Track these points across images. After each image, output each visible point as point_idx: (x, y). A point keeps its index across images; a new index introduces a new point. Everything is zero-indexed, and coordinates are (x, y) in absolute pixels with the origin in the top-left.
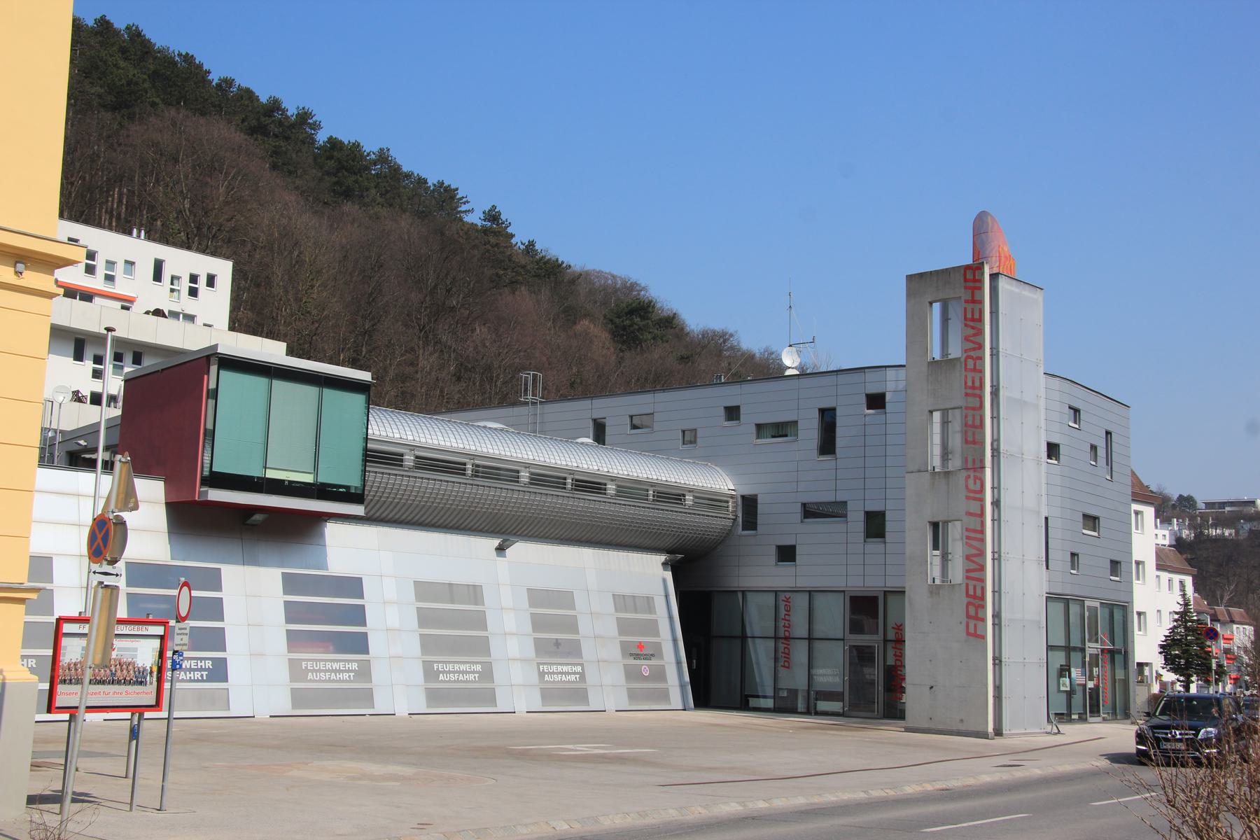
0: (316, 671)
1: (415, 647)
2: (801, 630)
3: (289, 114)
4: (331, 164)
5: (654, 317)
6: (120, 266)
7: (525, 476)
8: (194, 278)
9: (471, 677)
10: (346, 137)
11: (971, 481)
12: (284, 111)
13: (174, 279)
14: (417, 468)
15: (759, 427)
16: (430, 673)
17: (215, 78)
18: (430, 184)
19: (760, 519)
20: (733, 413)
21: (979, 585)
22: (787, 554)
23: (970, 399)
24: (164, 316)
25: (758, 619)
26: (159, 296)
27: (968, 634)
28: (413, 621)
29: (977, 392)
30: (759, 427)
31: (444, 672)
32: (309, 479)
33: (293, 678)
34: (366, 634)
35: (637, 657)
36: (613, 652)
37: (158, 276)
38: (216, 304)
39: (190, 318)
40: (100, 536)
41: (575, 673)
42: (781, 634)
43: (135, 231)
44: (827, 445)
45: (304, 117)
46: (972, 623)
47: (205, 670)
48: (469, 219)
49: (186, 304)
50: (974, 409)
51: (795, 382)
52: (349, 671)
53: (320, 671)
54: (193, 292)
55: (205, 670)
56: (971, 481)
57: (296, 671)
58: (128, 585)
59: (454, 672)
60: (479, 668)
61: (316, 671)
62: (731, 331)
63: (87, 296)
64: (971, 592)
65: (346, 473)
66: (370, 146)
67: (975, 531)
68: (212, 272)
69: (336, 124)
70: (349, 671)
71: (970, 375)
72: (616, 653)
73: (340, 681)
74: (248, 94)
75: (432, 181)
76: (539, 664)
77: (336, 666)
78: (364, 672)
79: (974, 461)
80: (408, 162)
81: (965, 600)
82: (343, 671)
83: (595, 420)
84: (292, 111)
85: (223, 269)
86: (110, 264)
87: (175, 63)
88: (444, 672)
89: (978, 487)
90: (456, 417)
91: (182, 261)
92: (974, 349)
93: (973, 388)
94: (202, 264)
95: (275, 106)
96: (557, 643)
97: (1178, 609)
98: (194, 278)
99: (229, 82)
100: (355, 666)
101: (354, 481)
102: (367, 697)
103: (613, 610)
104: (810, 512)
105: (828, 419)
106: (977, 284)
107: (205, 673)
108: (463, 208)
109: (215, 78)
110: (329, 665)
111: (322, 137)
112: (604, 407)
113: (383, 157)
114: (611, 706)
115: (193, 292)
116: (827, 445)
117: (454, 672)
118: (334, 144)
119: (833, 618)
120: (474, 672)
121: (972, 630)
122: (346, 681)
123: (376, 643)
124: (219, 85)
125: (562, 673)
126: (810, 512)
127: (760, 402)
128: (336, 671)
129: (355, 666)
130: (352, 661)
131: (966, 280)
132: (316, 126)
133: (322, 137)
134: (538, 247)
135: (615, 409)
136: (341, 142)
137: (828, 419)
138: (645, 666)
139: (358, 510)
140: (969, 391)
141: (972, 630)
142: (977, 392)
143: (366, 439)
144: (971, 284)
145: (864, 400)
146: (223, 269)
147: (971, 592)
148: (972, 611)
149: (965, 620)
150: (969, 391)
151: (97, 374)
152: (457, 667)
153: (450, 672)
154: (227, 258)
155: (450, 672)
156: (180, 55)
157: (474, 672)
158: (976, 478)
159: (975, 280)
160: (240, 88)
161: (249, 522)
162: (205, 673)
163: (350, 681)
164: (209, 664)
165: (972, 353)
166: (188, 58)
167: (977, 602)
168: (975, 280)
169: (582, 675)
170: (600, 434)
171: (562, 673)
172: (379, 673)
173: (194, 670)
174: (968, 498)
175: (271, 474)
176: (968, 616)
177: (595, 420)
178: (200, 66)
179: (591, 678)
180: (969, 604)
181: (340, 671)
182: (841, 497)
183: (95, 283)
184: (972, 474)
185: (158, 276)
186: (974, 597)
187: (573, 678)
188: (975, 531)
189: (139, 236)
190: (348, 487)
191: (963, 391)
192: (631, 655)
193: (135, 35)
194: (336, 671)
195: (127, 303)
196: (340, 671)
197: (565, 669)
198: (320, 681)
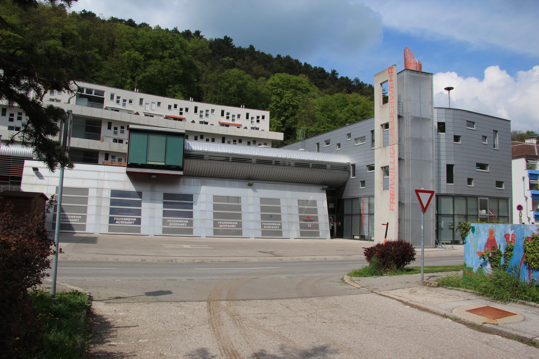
1: (259, 218)
6: (261, 118)
7: (254, 161)
8: (258, 117)
9: (233, 226)
13: (252, 118)
16: (216, 224)
19: (455, 179)
20: (349, 135)
26: (247, 123)
28: (259, 210)
32: (163, 164)
33: (214, 226)
36: (296, 219)
37: (247, 118)
38: (265, 124)
46: (391, 204)
49: (256, 125)
54: (258, 121)
57: (165, 222)
60: (236, 223)
63: (227, 125)
68: (187, 107)
71: (391, 109)
72: (297, 219)
76: (262, 223)
78: (191, 223)
81: (390, 196)
85: (267, 114)
86: (233, 116)
90: (286, 147)
91: (254, 113)
94: (260, 113)
96: (271, 216)
98: (258, 117)
110: (177, 221)
111: (339, 77)
113: (357, 80)
114: (203, 235)
115: (258, 121)
128: (180, 223)
130: (186, 220)
139: (181, 173)
143: (184, 151)
146: (267, 114)
149: (389, 204)
176: (391, 203)
179: (284, 227)
180: (391, 198)
181: (181, 223)
183: (229, 121)
185: (247, 118)
193: (288, 58)
194: (180, 223)
195: (239, 126)
196: (181, 223)
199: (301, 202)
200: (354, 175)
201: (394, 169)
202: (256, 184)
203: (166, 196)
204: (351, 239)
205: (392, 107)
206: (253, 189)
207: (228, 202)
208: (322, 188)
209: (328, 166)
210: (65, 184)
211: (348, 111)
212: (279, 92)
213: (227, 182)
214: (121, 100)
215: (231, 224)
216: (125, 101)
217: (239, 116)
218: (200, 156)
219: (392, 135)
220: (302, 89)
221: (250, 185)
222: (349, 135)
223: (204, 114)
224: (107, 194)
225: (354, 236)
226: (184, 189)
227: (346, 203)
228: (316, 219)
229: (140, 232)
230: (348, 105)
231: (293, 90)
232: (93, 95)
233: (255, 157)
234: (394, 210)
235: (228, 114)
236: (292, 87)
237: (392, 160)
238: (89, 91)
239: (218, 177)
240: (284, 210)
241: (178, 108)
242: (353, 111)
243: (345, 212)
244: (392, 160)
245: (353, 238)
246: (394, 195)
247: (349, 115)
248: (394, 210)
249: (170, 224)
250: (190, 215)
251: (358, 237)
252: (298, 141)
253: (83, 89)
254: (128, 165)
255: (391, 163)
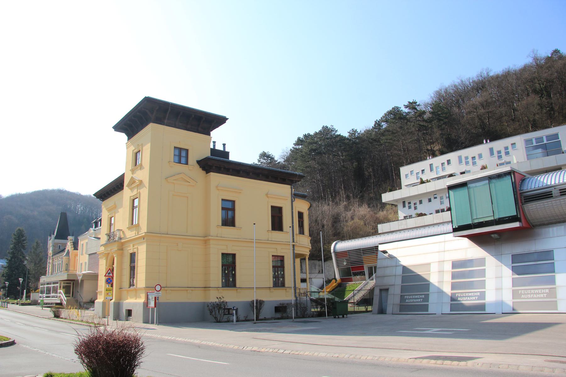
0: (526, 294)
14: (561, 195)
32: (492, 218)
43: (484, 141)
47: (545, 293)
55: (545, 293)
60: (423, 296)
61: (526, 294)
73: (538, 298)
77: (536, 291)
102: (554, 304)
107: (545, 295)
122: (542, 298)
128: (536, 294)
129: (478, 294)
151: (442, 203)
152: (414, 297)
162: (545, 295)
163: (544, 298)
164: (478, 294)
166: (300, 141)
173: (540, 294)
175: (476, 221)
181: (417, 298)
189: (487, 142)
194: (536, 294)
196: (538, 293)
198: (528, 298)
200: (301, 215)
203: (515, 258)
207: (320, 242)
210: (296, 252)
214: (470, 160)
216: (473, 158)
217: (480, 156)
218: (545, 195)
223: (503, 154)
224: (448, 267)
229: (485, 310)
232: (545, 142)
235: (467, 158)
238: (539, 139)
241: (415, 173)
249: (523, 296)
253: (531, 140)
254: (453, 229)
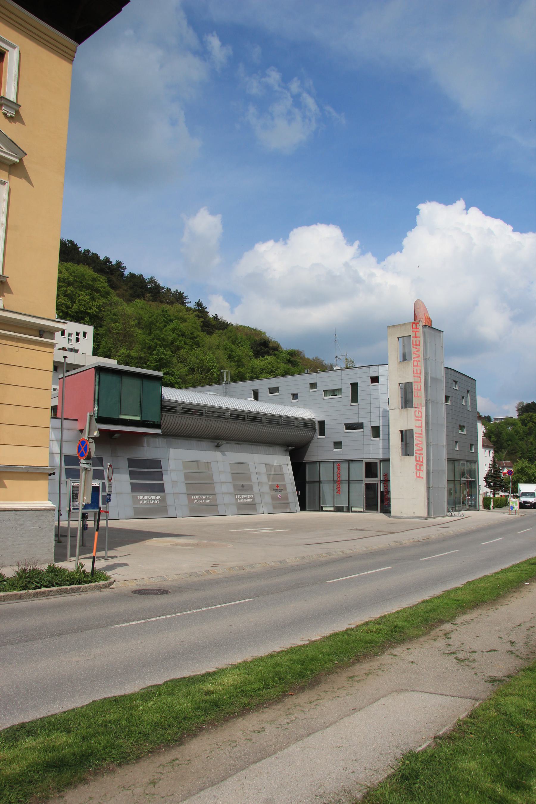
0: (144, 500)
2: (344, 477)
3: (113, 263)
4: (131, 284)
5: (271, 345)
6: (81, 335)
7: (179, 409)
8: (78, 334)
9: (208, 501)
10: (136, 272)
11: (417, 413)
12: (111, 262)
13: (70, 335)
15: (325, 391)
17: (82, 250)
18: (172, 291)
19: (326, 431)
21: (421, 456)
22: (338, 444)
23: (416, 378)
24: (66, 350)
25: (326, 473)
27: (417, 477)
29: (419, 375)
30: (324, 391)
31: (196, 499)
32: (138, 418)
34: (131, 479)
35: (276, 490)
36: (266, 489)
38: (87, 345)
39: (76, 351)
40: (82, 448)
41: (251, 498)
42: (336, 479)
44: (354, 398)
45: (119, 264)
46: (418, 472)
48: (188, 305)
49: (74, 345)
50: (417, 382)
51: (339, 373)
52: (157, 500)
53: (145, 500)
54: (78, 340)
56: (417, 413)
58: (65, 465)
59: (200, 499)
61: (144, 500)
62: (301, 350)
64: (418, 459)
65: (153, 416)
66: (147, 276)
67: (419, 434)
68: (85, 331)
69: (132, 267)
70: (157, 500)
71: (415, 368)
74: (96, 256)
75: (173, 290)
79: (418, 405)
80: (161, 283)
81: (415, 463)
82: (155, 500)
83: (253, 390)
84: (114, 263)
87: (67, 244)
88: (196, 499)
89: (420, 415)
92: (417, 357)
93: (417, 373)
94: (81, 328)
95: (107, 260)
97: (491, 463)
98: (78, 334)
99: (87, 251)
100: (159, 497)
101: (157, 420)
103: (265, 471)
104: (349, 427)
105: (354, 386)
106: (418, 330)
108: (187, 301)
109: (82, 250)
111: (126, 273)
112: (256, 384)
113: (152, 281)
115: (78, 340)
116: (354, 398)
117: (200, 499)
118: (132, 275)
119: (359, 472)
120: (209, 499)
121: (418, 475)
123: (167, 488)
124: (84, 253)
125: (245, 498)
126: (349, 427)
127: (325, 380)
128: (152, 500)
131: (413, 328)
132: (124, 268)
133: (126, 273)
134: (219, 317)
135: (263, 385)
136: (135, 275)
137: (354, 386)
138: (280, 495)
139: (159, 431)
140: (415, 375)
141: (418, 475)
142: (419, 375)
144: (415, 330)
145: (370, 380)
146: (90, 330)
147: (418, 459)
148: (418, 467)
149: (415, 471)
150: (415, 375)
153: (199, 499)
154: (91, 325)
155: (199, 499)
156: (68, 241)
157: (209, 499)
158: (419, 411)
159: (416, 328)
160: (92, 254)
161: (113, 437)
165: (416, 359)
167: (420, 463)
168: (416, 328)
169: (254, 499)
170: (256, 396)
171: (245, 498)
172: (170, 501)
174: (416, 420)
175: (123, 417)
176: (417, 469)
177: (253, 390)
178: (76, 245)
180: (416, 464)
182: (360, 421)
184: (417, 409)
186: (419, 461)
187: (250, 500)
188: (419, 434)
190: (154, 422)
191: (413, 375)
192: (274, 490)
196: (153, 500)
197: (246, 496)
199: (268, 466)
201: (422, 434)
202: (225, 446)
203: (132, 463)
204: (319, 511)
205: (417, 366)
206: (221, 452)
208: (286, 449)
209: (264, 419)
211: (174, 330)
212: (69, 292)
213: (194, 443)
215: (206, 499)
219: (418, 396)
220: (100, 290)
221: (218, 446)
222: (313, 386)
225: (322, 507)
226: (149, 451)
227: (308, 467)
228: (285, 488)
230: (171, 321)
231: (89, 291)
233: (180, 403)
234: (422, 478)
236: (88, 287)
237: (418, 423)
239: (233, 440)
240: (254, 479)
242: (180, 331)
243: (307, 479)
244: (418, 423)
245: (321, 510)
246: (422, 462)
247: (175, 335)
248: (422, 478)
250: (161, 489)
251: (332, 509)
252: (222, 383)
255: (416, 426)
